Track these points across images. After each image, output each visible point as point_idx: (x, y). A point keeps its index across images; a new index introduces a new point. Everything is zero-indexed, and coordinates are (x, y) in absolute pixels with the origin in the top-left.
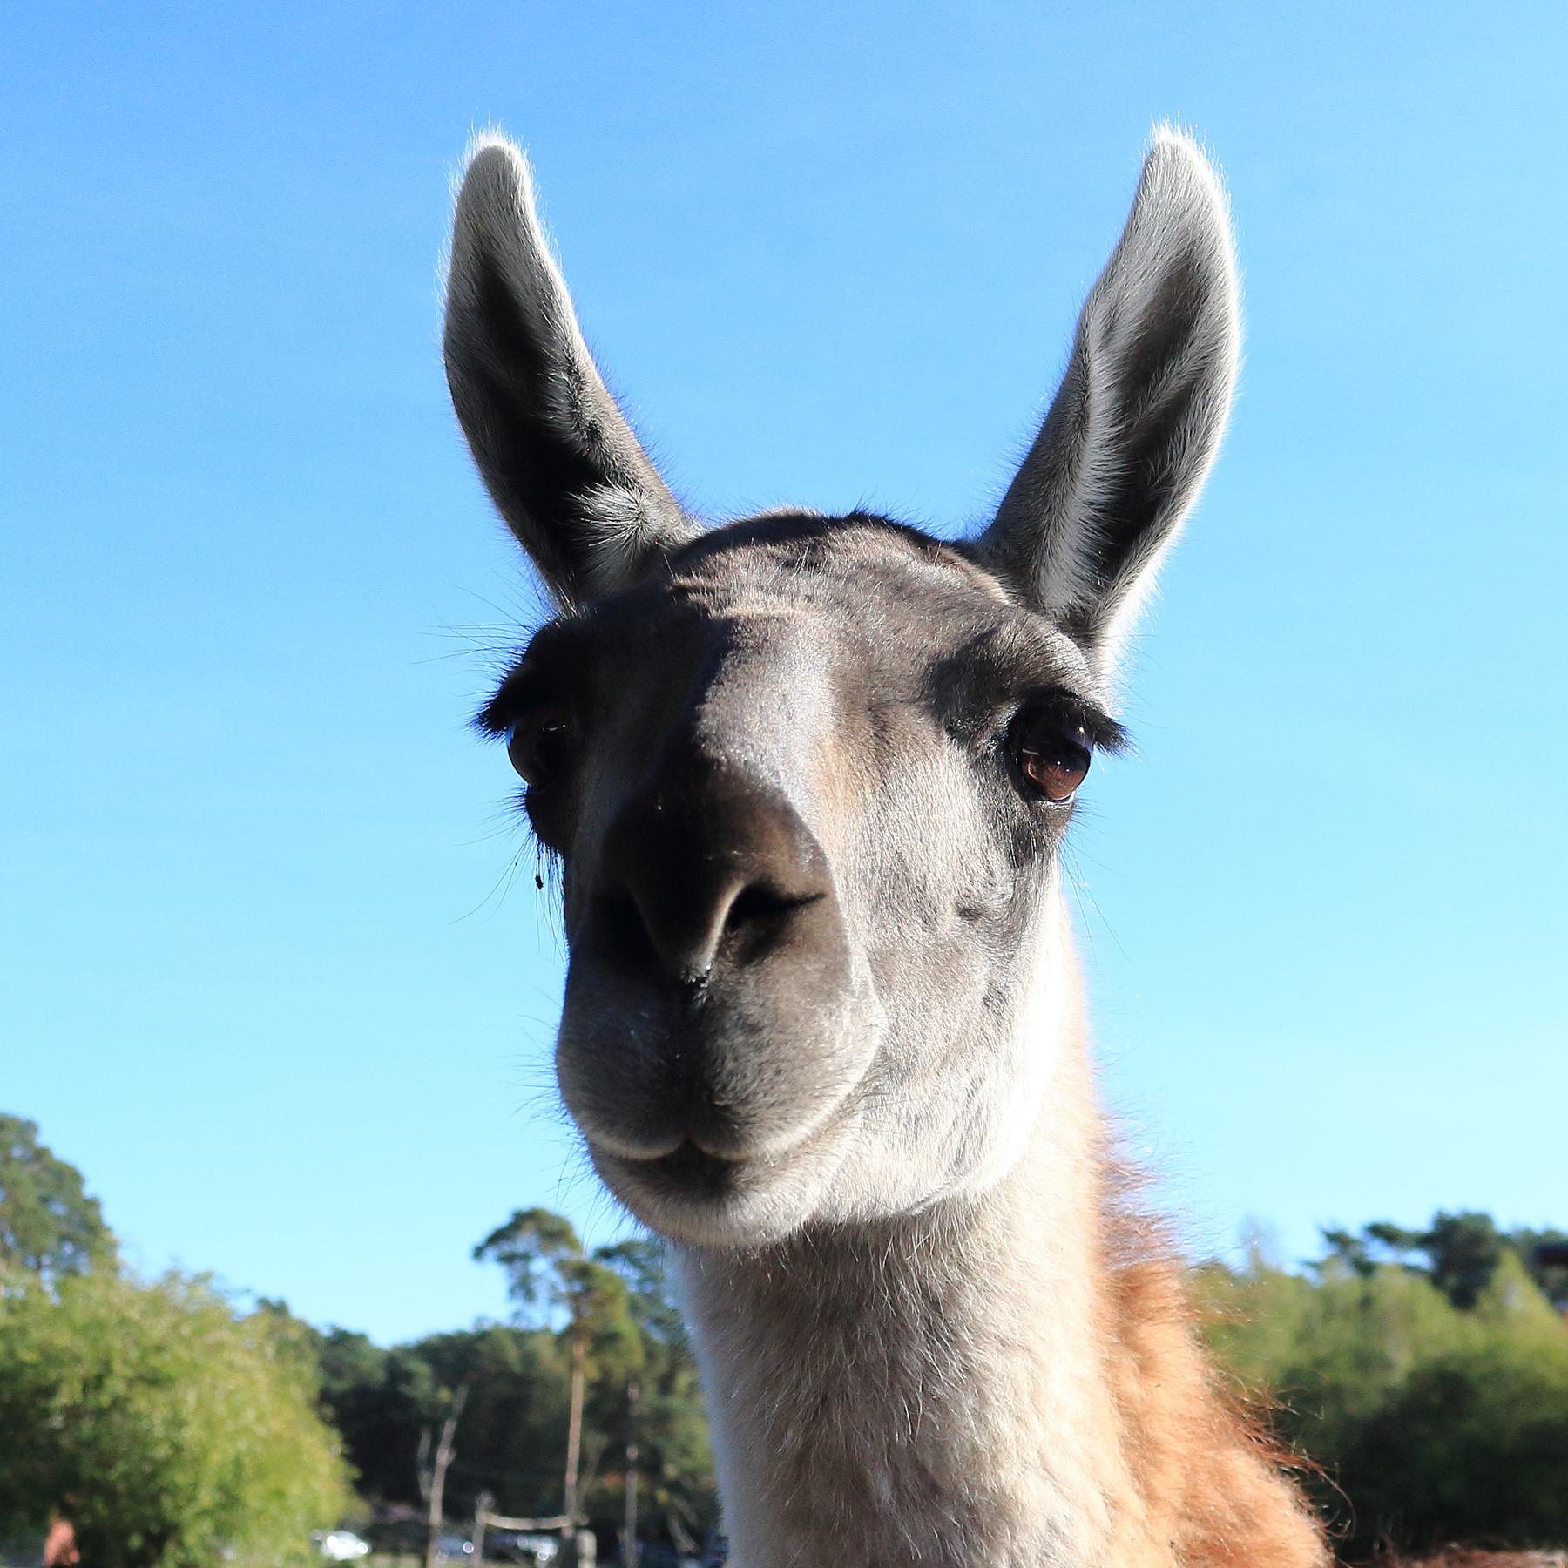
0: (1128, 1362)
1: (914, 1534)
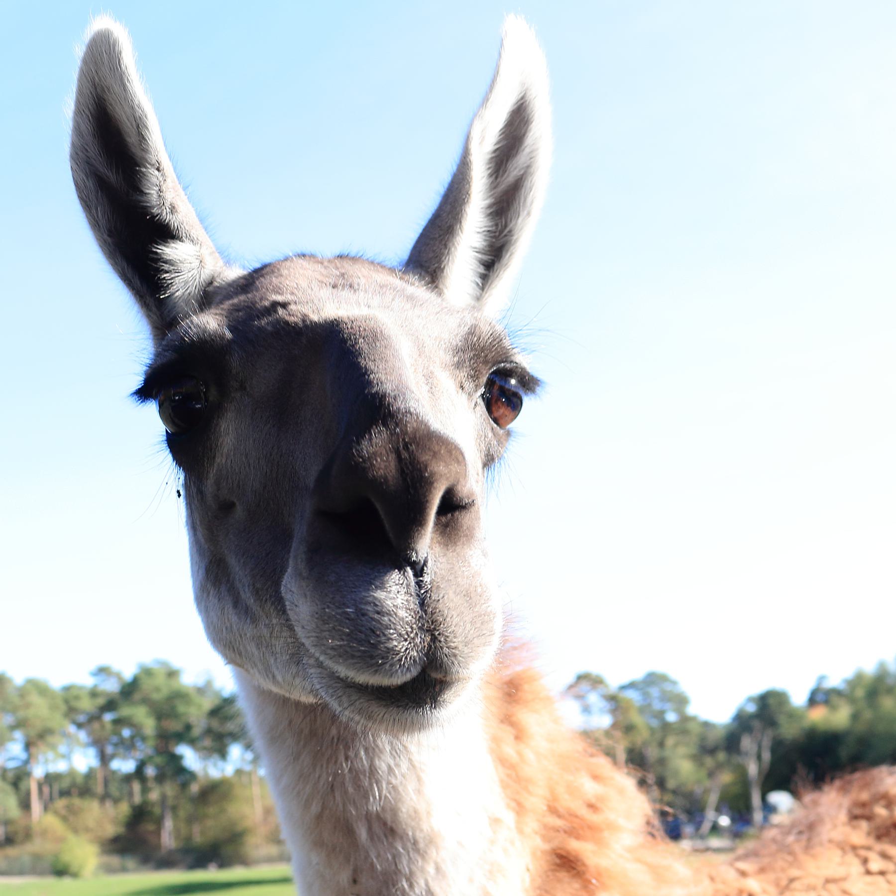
0: (507, 733)
1: (378, 856)
